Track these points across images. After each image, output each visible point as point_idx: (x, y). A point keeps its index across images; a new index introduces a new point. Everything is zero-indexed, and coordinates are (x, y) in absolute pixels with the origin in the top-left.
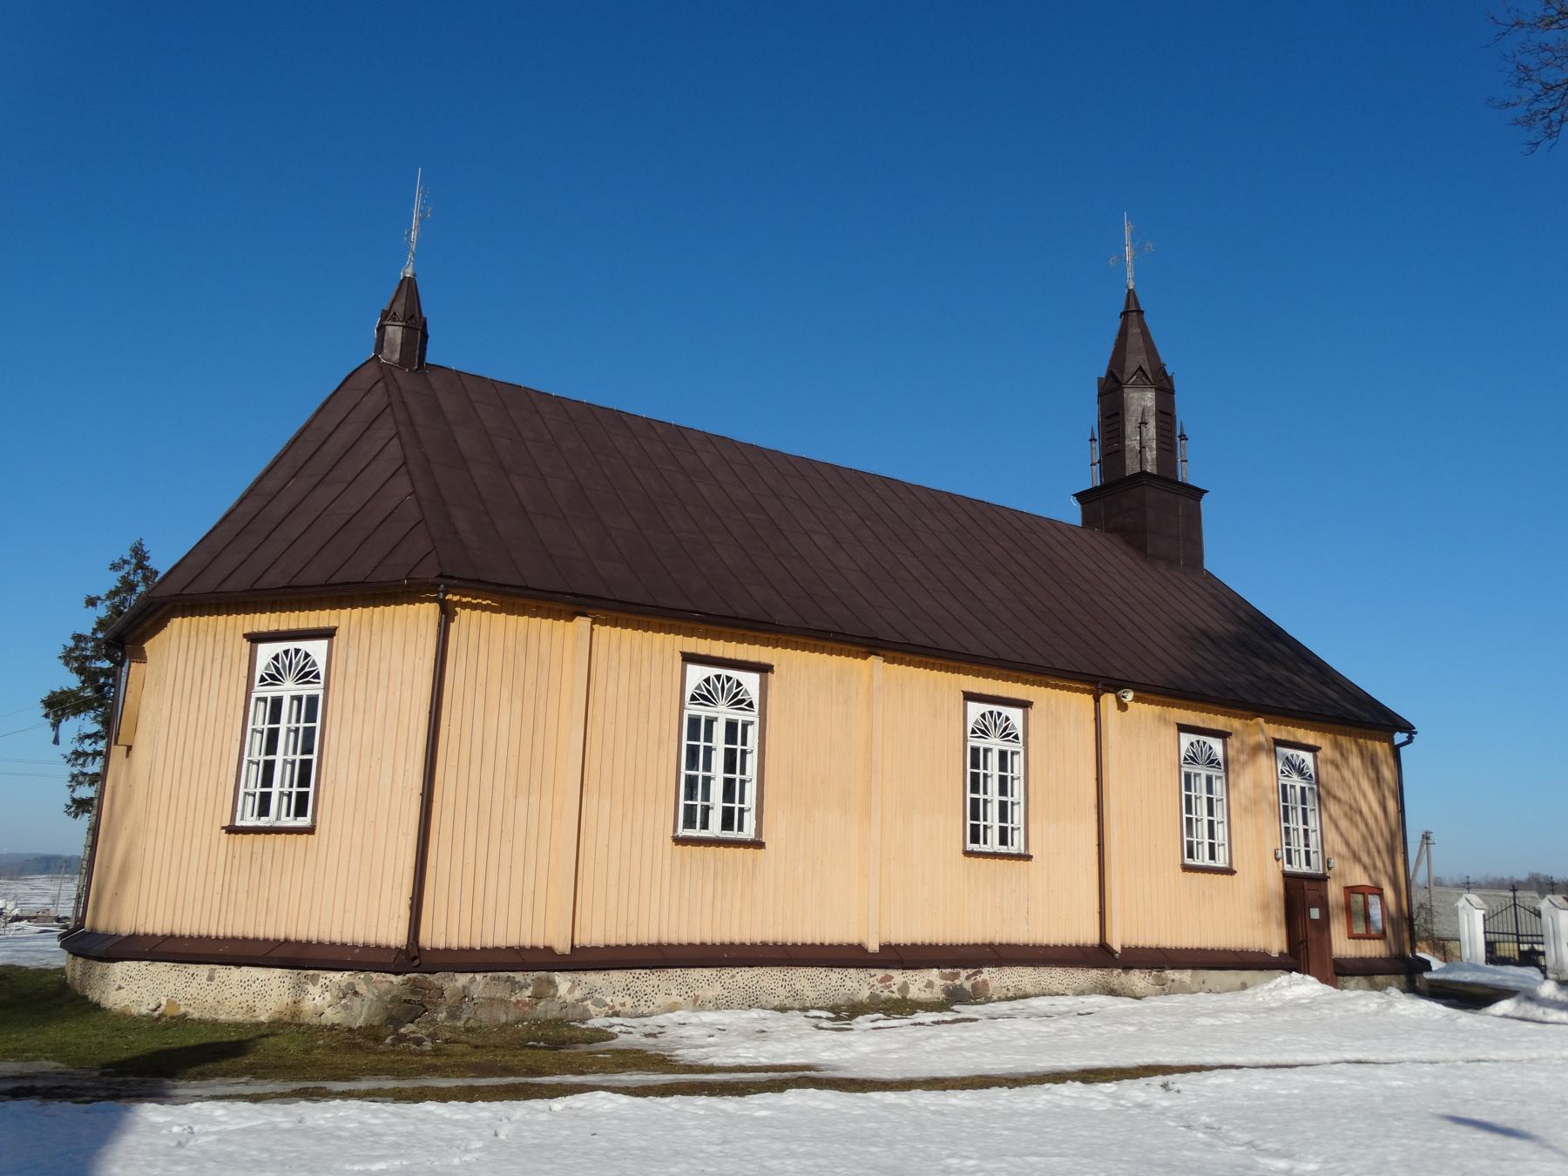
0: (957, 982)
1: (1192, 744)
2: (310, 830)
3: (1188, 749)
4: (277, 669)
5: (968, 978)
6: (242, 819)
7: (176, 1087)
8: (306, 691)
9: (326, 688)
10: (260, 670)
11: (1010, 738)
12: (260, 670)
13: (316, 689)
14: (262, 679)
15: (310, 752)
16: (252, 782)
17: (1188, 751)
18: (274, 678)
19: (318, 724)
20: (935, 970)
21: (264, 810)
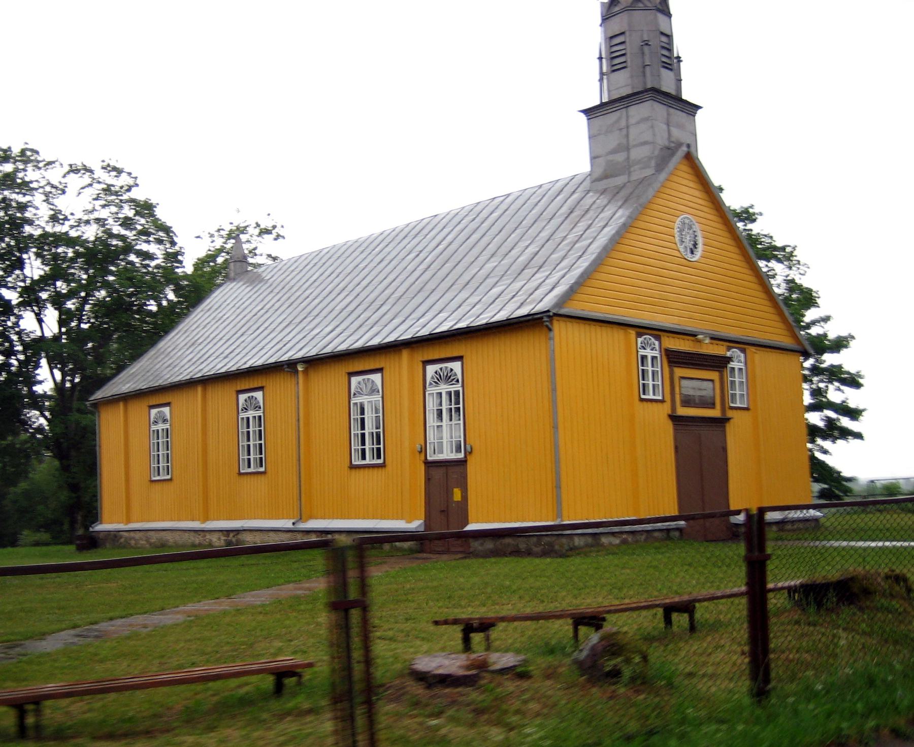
0: (229, 538)
1: (246, 401)
2: (383, 466)
3: (356, 387)
4: (361, 389)
5: (234, 536)
6: (355, 461)
7: (524, 730)
8: (453, 388)
9: (463, 386)
10: (152, 420)
11: (453, 382)
12: (152, 420)
13: (458, 387)
14: (431, 384)
15: (261, 427)
16: (356, 446)
17: (243, 405)
18: (245, 409)
19: (262, 428)
20: (41, 361)
21: (364, 458)
